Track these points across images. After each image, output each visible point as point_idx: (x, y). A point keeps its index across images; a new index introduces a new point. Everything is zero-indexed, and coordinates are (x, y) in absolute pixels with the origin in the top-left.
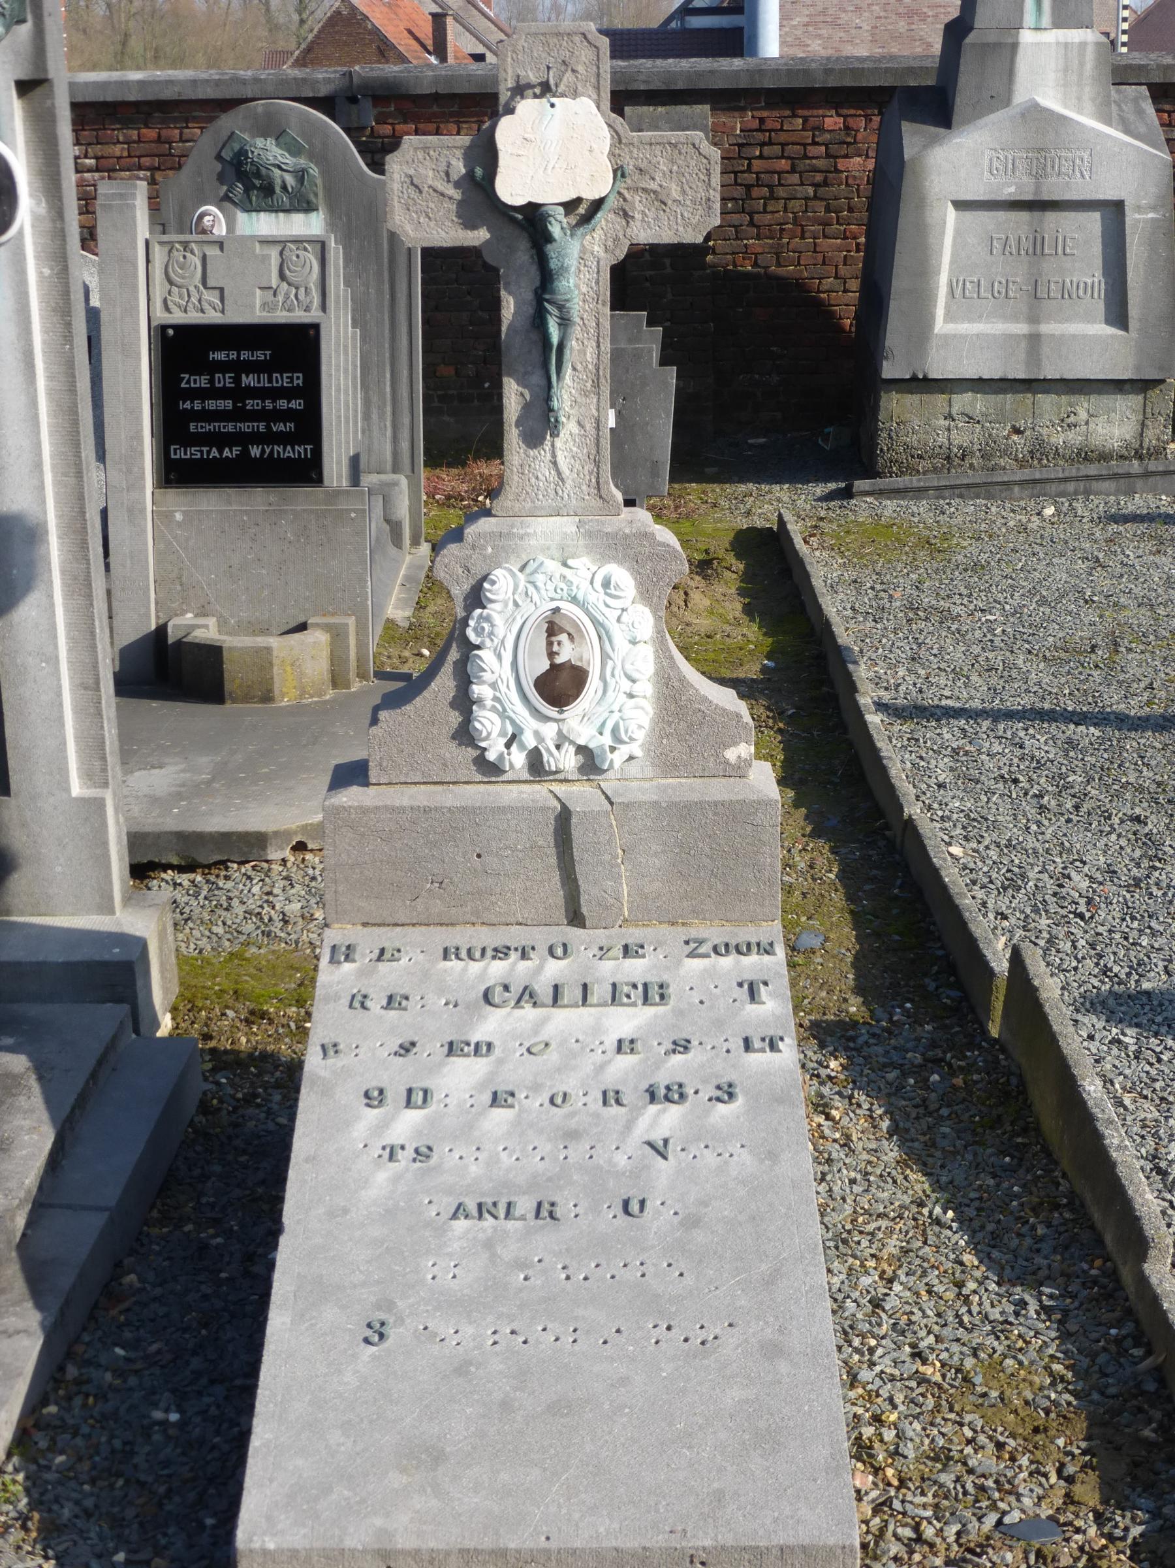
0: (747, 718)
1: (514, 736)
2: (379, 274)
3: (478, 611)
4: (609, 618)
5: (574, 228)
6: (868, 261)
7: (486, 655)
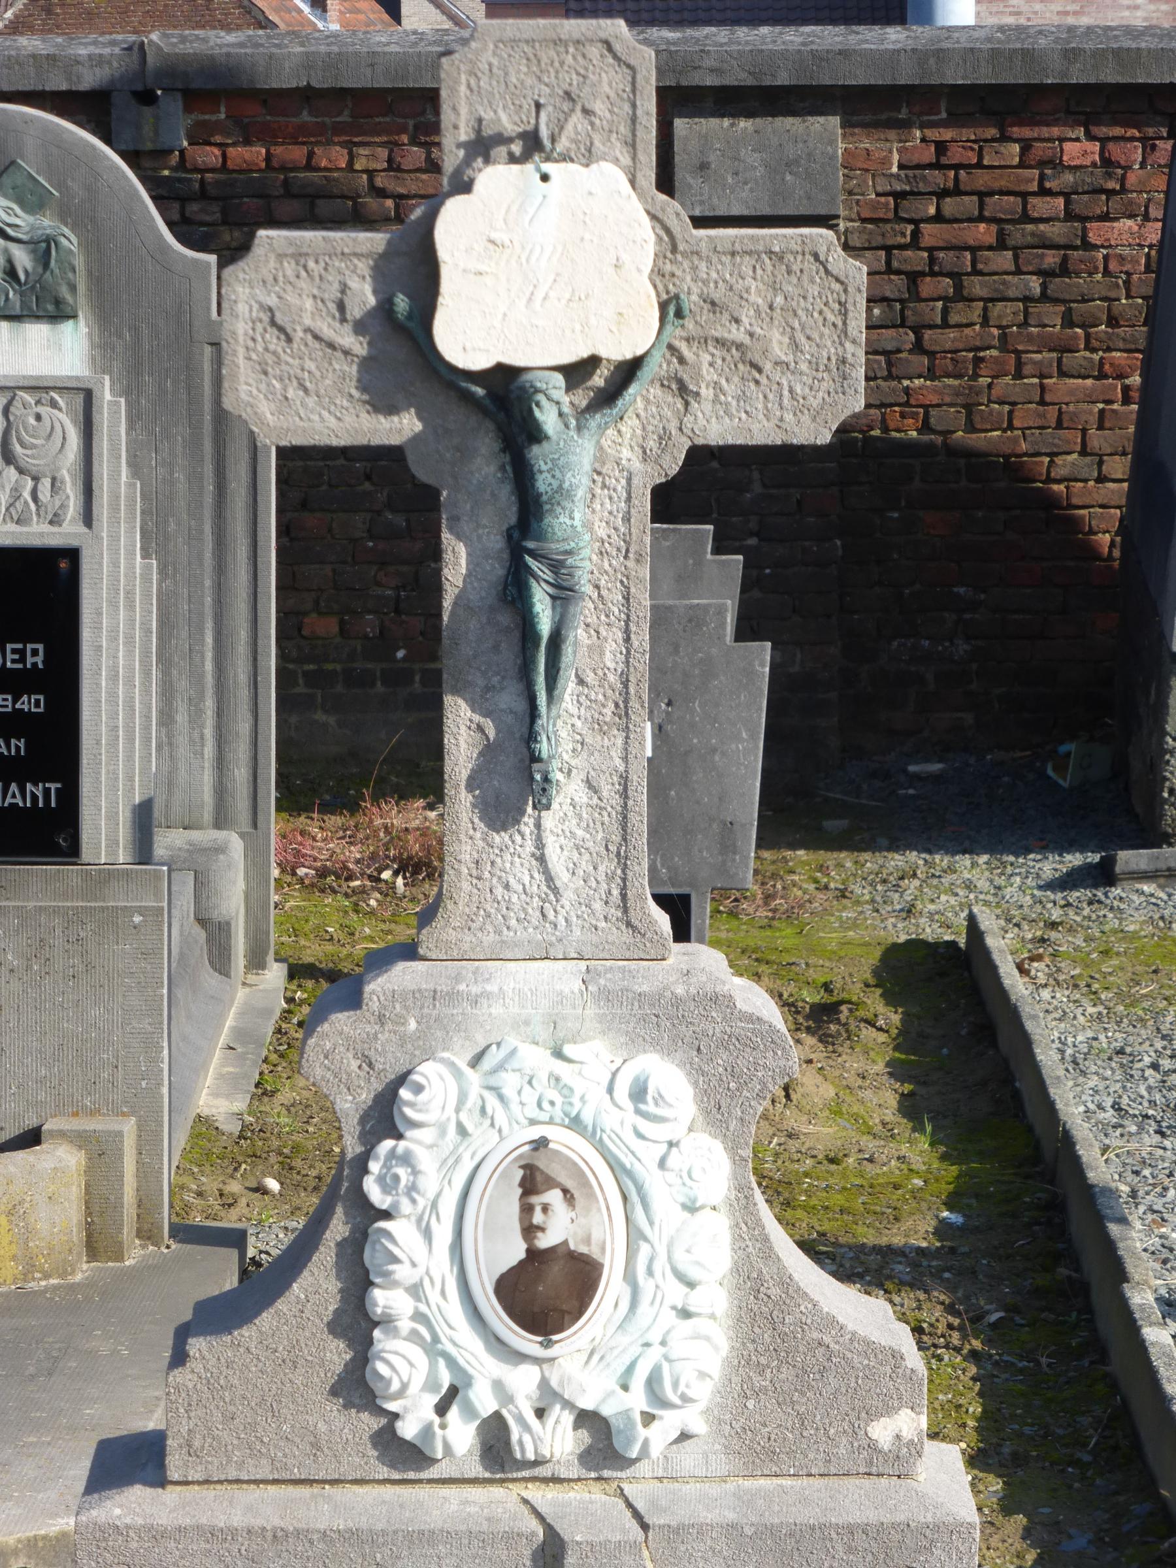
0: (903, 1339)
1: (453, 1391)
2: (194, 443)
3: (388, 1144)
4: (643, 1160)
5: (584, 413)
6: (1143, 421)
7: (402, 1230)
